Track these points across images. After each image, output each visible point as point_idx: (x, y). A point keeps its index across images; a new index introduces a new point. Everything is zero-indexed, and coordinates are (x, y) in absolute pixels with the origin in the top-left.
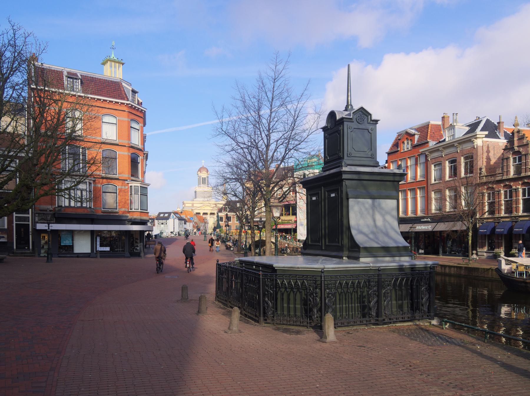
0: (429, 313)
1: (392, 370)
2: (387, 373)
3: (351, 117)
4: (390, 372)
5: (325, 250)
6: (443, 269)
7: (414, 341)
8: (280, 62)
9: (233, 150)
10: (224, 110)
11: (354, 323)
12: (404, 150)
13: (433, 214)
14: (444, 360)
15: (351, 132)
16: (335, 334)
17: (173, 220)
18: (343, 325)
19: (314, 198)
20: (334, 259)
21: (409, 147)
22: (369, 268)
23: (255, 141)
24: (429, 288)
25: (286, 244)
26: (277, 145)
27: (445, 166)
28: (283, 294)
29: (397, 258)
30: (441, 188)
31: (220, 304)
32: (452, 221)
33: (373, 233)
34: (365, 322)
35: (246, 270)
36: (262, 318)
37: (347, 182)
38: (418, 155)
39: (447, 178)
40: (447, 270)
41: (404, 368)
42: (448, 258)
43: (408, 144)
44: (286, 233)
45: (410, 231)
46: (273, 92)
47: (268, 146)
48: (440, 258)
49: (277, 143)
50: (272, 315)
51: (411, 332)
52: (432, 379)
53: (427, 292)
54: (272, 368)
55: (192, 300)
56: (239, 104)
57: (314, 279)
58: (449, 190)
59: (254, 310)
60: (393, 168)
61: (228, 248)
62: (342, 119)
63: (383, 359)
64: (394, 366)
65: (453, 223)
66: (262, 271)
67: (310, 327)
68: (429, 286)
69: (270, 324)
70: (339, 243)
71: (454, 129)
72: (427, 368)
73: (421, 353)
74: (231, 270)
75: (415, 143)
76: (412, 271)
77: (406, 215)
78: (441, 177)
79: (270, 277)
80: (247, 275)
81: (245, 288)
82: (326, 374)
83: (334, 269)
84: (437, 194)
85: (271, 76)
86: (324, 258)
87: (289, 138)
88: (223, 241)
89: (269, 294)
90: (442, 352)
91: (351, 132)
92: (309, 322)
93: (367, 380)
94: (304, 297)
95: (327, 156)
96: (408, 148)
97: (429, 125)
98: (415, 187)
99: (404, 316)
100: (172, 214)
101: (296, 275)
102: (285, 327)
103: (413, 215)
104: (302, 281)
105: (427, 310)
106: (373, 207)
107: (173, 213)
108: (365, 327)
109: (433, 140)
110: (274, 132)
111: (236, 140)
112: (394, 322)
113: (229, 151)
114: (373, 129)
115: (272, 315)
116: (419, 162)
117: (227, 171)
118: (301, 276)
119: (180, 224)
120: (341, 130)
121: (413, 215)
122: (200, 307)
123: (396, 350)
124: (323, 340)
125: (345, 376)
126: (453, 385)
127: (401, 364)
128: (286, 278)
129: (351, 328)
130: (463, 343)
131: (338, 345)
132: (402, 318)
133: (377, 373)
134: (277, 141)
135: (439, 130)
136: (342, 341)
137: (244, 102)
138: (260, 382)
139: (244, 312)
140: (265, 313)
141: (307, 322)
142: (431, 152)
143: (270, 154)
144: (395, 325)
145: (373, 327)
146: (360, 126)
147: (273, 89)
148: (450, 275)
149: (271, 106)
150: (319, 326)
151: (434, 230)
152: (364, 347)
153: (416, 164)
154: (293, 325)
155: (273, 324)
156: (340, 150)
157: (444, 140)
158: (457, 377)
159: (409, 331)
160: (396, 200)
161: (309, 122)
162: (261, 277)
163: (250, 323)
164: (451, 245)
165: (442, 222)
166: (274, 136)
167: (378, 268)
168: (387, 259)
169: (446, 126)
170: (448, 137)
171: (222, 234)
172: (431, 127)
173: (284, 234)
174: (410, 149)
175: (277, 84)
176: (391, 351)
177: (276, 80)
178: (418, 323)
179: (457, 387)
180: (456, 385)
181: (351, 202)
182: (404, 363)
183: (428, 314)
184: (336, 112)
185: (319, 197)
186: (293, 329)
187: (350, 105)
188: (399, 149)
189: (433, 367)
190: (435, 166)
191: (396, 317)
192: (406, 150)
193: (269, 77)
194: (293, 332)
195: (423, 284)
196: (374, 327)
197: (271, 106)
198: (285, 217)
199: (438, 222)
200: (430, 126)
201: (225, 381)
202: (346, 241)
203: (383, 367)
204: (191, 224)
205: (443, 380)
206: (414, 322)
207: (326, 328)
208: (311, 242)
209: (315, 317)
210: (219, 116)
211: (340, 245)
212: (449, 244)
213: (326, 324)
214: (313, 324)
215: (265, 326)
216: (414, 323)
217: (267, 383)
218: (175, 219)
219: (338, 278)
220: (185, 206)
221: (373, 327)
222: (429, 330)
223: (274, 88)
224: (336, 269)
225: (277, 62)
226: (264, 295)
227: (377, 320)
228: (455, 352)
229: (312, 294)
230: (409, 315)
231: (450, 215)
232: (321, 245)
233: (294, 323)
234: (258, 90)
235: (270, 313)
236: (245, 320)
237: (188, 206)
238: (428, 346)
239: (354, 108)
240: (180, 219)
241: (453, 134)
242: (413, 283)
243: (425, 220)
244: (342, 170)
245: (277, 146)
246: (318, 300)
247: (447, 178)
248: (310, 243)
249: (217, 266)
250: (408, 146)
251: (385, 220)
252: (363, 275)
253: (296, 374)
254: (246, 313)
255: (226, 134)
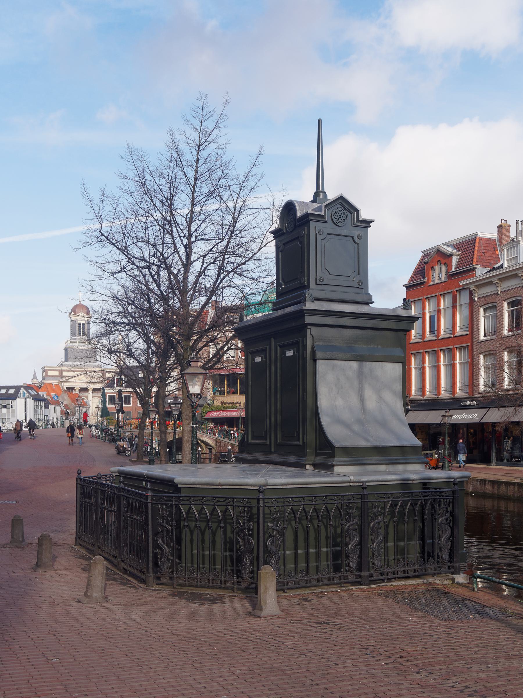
0: (450, 562)
1: (366, 665)
2: (356, 671)
3: (323, 213)
4: (364, 668)
5: (276, 452)
6: (496, 488)
7: (420, 613)
8: (209, 115)
9: (122, 270)
10: (105, 198)
11: (318, 581)
12: (434, 281)
13: (482, 393)
14: (464, 645)
15: (322, 240)
16: (278, 602)
17: (23, 400)
18: (297, 586)
19: (258, 359)
20: (290, 469)
21: (443, 276)
22: (348, 484)
23: (162, 254)
24: (451, 518)
25: (228, 445)
26: (203, 264)
27: (502, 311)
28: (214, 533)
29: (400, 467)
30: (495, 348)
31: (83, 551)
32: (511, 407)
33: (359, 422)
34: (337, 580)
35: (124, 489)
36: (151, 575)
37: (314, 330)
38: (457, 291)
39: (506, 332)
40: (503, 490)
41: (389, 662)
42: (505, 470)
43: (441, 271)
44: (229, 426)
45: (442, 422)
46: (197, 168)
47: (187, 265)
48: (492, 468)
49: (203, 260)
50: (170, 570)
51: (416, 596)
52: (435, 679)
53: (447, 526)
54: (147, 665)
55: (32, 544)
56: (134, 187)
57: (247, 505)
58: (508, 352)
59: (139, 561)
60: (415, 312)
61: (120, 451)
62: (307, 217)
63: (356, 645)
64: (373, 657)
65: (513, 408)
66: (152, 490)
67: (239, 589)
68: (452, 514)
69: (167, 585)
70: (299, 440)
71: (517, 247)
72: (431, 660)
73: (425, 633)
74: (100, 490)
75: (451, 269)
76: (424, 488)
77: (436, 395)
78: (496, 330)
79: (166, 501)
80: (127, 497)
81: (124, 521)
82: (246, 674)
83: (285, 487)
84: (488, 358)
85: (193, 139)
86: (272, 467)
87: (224, 252)
88: (113, 439)
89: (165, 533)
90: (463, 631)
91: (322, 240)
92: (223, 581)
93: (317, 684)
94: (230, 538)
95: (281, 282)
96: (440, 279)
97: (475, 240)
98: (452, 347)
99: (406, 568)
100: (22, 390)
101: (214, 497)
102: (193, 590)
103: (448, 395)
104: (224, 508)
105: (447, 557)
106: (361, 375)
107: (24, 387)
108: (337, 589)
109: (483, 266)
110: (199, 240)
111: (127, 252)
112: (390, 580)
113: (116, 273)
114: (361, 237)
115: (170, 570)
116: (460, 303)
117: (115, 310)
118: (223, 499)
119: (36, 408)
120: (303, 236)
121: (448, 395)
122: (39, 556)
123: (383, 628)
124: (257, 612)
125: (280, 677)
126: (470, 690)
127: (387, 653)
128: (219, 503)
129: (312, 590)
130: (503, 614)
131: (280, 621)
132: (404, 572)
133: (339, 670)
134: (204, 256)
135: (492, 249)
136: (289, 614)
137: (143, 184)
138: (117, 692)
139: (123, 564)
140: (156, 565)
141: (221, 581)
142: (478, 287)
143: (191, 279)
144: (390, 584)
145: (351, 588)
146: (340, 231)
147: (197, 163)
148: (507, 498)
149: (193, 193)
150: (252, 588)
151: (482, 421)
152: (327, 624)
153: (454, 307)
154: (208, 587)
155: (173, 585)
156: (302, 272)
157: (502, 266)
158: (482, 675)
159: (413, 595)
160: (400, 364)
161: (262, 224)
162: (150, 501)
163: (130, 584)
164: (511, 448)
165: (495, 407)
166: (199, 248)
167: (361, 484)
168: (383, 468)
169: (505, 241)
170: (508, 260)
171: (111, 427)
172: (479, 243)
173: (226, 427)
174: (443, 279)
175: (204, 154)
176: (373, 630)
177: (201, 147)
178: (431, 580)
179: (476, 694)
180: (476, 691)
181: (321, 365)
182: (391, 652)
183: (449, 564)
184: (296, 204)
185: (266, 358)
186: (207, 594)
187: (322, 192)
188: (425, 280)
189: (441, 659)
190: (485, 310)
191: (393, 570)
192: (437, 281)
193: (189, 142)
194: (205, 599)
195: (441, 511)
196: (353, 588)
197: (193, 193)
198: (228, 397)
199: (490, 408)
200: (477, 240)
201: (50, 692)
202: (311, 437)
203: (352, 659)
204: (58, 408)
205: (454, 681)
206: (424, 579)
207: (262, 591)
208: (252, 439)
209: (247, 572)
210: (96, 208)
211: (301, 444)
212: (508, 444)
213: (262, 584)
214: (243, 585)
215: (156, 590)
216: (425, 581)
217: (131, 693)
218: (28, 400)
219: (289, 502)
220: (46, 375)
221: (351, 588)
222: (449, 593)
223: (198, 159)
224: (288, 487)
225: (204, 113)
226: (156, 534)
227: (360, 576)
228: (486, 630)
229: (242, 530)
230: (417, 567)
231: (509, 395)
232: (268, 443)
233: (209, 583)
234: (168, 163)
235: (166, 566)
236: (123, 578)
237: (52, 376)
238: (442, 620)
239: (328, 198)
240: (38, 399)
241: (515, 256)
242: (425, 511)
243: (468, 403)
244: (304, 308)
245: (204, 266)
246: (253, 541)
247: (506, 332)
248: (250, 440)
249: (79, 482)
250: (441, 275)
251: (381, 399)
252: (335, 496)
253: (190, 676)
254: (126, 567)
255: (109, 241)
